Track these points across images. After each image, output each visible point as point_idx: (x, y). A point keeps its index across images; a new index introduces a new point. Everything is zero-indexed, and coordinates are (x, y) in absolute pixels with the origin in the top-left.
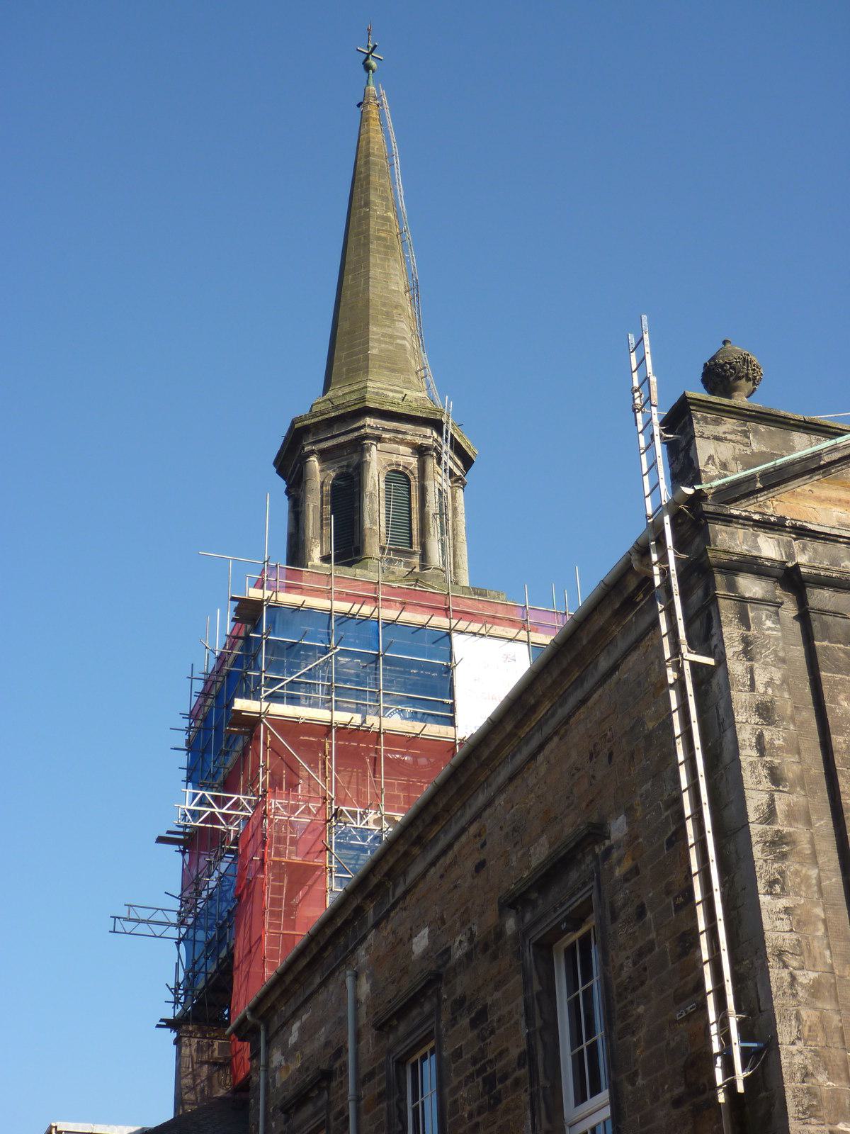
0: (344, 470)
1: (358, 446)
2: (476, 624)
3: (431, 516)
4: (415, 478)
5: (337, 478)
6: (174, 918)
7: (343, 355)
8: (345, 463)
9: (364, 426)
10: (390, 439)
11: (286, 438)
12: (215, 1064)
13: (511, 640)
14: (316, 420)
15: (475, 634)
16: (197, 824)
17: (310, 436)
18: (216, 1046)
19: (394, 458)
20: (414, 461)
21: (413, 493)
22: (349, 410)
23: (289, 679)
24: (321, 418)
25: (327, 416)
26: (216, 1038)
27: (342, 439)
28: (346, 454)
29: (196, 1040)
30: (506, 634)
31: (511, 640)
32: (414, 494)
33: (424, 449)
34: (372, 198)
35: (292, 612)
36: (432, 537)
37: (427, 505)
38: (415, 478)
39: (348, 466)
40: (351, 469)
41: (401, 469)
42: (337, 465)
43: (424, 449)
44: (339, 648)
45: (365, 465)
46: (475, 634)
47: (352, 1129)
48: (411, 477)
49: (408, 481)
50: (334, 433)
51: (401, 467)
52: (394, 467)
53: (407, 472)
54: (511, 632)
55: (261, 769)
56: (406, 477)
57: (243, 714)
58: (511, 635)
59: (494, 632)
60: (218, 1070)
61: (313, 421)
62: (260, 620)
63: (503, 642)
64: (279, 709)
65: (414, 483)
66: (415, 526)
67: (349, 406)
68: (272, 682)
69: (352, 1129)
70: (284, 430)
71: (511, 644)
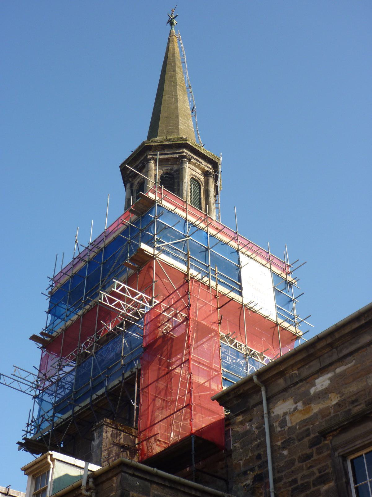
0: (169, 171)
1: (180, 161)
2: (49, 338)
3: (212, 204)
4: (203, 185)
5: (164, 173)
6: (33, 379)
7: (164, 126)
8: (169, 168)
9: (184, 152)
10: (193, 163)
11: (134, 153)
12: (122, 447)
13: (263, 265)
14: (157, 144)
15: (249, 256)
16: (118, 301)
17: (151, 152)
18: (122, 436)
19: (194, 173)
20: (202, 178)
21: (202, 191)
22: (177, 142)
23: (167, 243)
24: (160, 144)
25: (164, 143)
26: (123, 431)
27: (170, 156)
28: (170, 164)
29: (111, 429)
30: (261, 261)
31: (263, 265)
32: (203, 192)
33: (208, 173)
34: (177, 69)
35: (168, 212)
36: (213, 213)
37: (210, 198)
38: (203, 185)
39: (171, 170)
40: (173, 171)
41: (197, 179)
42: (164, 168)
43: (208, 173)
44: (190, 238)
45: (184, 169)
46: (249, 256)
47: (272, 495)
48: (201, 184)
49: (200, 186)
50: (166, 152)
51: (197, 178)
52: (194, 177)
53: (199, 181)
54: (264, 262)
55: (154, 283)
56: (199, 183)
57: (145, 252)
58: (264, 264)
59: (256, 258)
60: (123, 451)
61: (155, 144)
62: (153, 207)
63: (260, 265)
64: (163, 257)
65: (202, 188)
66: (203, 206)
67: (177, 141)
68: (159, 242)
69: (272, 495)
70: (142, 142)
71: (263, 267)
